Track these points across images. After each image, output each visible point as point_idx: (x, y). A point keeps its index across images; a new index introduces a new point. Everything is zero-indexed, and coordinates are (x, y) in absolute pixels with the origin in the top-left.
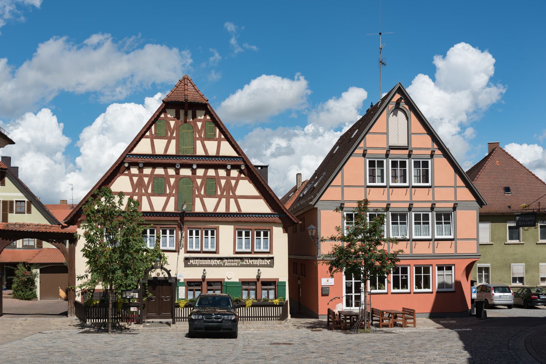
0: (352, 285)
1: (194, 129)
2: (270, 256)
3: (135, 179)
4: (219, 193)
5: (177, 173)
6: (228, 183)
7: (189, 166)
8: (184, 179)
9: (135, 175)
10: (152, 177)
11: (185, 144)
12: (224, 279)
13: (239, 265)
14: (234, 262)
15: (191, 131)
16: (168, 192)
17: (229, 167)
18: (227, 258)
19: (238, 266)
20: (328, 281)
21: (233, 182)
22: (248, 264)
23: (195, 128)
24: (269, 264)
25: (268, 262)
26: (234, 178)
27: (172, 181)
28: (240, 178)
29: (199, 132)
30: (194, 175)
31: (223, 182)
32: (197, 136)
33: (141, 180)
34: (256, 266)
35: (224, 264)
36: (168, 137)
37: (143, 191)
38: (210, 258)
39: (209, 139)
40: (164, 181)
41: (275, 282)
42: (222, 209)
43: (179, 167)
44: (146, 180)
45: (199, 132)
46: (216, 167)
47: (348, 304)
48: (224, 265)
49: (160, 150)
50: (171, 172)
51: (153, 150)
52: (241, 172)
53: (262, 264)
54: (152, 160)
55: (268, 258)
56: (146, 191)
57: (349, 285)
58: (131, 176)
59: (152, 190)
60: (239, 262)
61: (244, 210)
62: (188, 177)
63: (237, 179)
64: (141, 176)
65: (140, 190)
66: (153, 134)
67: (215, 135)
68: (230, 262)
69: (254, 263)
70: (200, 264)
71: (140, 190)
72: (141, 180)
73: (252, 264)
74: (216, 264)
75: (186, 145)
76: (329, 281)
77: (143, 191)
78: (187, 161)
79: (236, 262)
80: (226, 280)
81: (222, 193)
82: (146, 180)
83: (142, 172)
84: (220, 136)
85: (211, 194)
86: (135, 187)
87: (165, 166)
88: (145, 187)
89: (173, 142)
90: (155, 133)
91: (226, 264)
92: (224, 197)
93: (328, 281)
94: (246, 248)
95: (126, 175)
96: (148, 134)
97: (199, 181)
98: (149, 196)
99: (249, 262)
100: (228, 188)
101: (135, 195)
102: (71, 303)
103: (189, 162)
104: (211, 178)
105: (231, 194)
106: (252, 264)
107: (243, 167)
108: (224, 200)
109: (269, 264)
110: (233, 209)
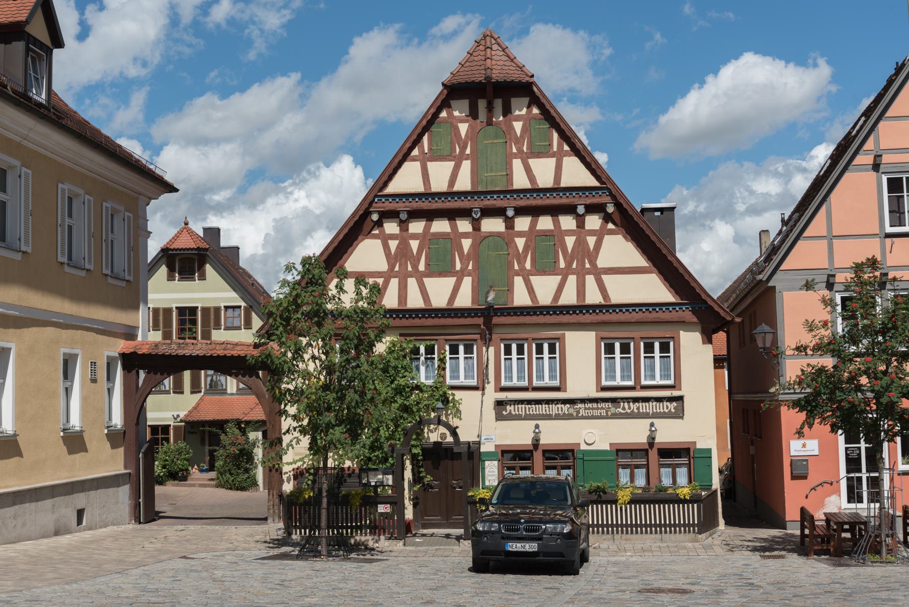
0: (860, 454)
1: (508, 137)
2: (676, 393)
3: (393, 245)
4: (562, 264)
5: (477, 228)
6: (581, 243)
7: (498, 212)
8: (490, 238)
9: (393, 237)
10: (426, 238)
11: (489, 168)
12: (579, 444)
13: (609, 413)
14: (598, 409)
15: (501, 141)
16: (458, 266)
17: (510, 213)
18: (583, 401)
19: (607, 417)
20: (804, 446)
21: (591, 241)
22: (629, 411)
23: (510, 134)
24: (673, 410)
25: (672, 406)
26: (592, 233)
27: (466, 244)
28: (605, 232)
29: (518, 141)
30: (511, 231)
31: (570, 241)
32: (514, 150)
33: (404, 247)
34: (646, 416)
35: (578, 412)
36: (455, 157)
37: (410, 269)
38: (548, 402)
39: (539, 155)
40: (449, 245)
41: (689, 449)
42: (569, 297)
43: (479, 215)
44: (414, 245)
45: (518, 141)
46: (555, 211)
47: (854, 495)
48: (577, 415)
49: (439, 184)
50: (464, 226)
51: (427, 183)
52: (607, 218)
53: (658, 411)
54: (425, 205)
55: (671, 399)
56: (415, 267)
57: (854, 455)
58: (385, 239)
59: (427, 265)
60: (609, 408)
61: (615, 299)
62: (498, 235)
63: (600, 235)
64: (404, 237)
65: (403, 266)
66: (426, 151)
67: (551, 145)
68: (589, 409)
69: (641, 411)
70: (528, 413)
71: (403, 266)
72: (404, 247)
73: (636, 411)
74: (560, 412)
75: (491, 171)
76: (807, 446)
77: (410, 269)
78: (494, 202)
79: (602, 408)
80: (583, 447)
81: (569, 264)
82: (414, 245)
83: (407, 230)
84: (560, 146)
85: (545, 268)
86: (568, 258)
87: (452, 215)
88: (412, 259)
89: (466, 165)
90: (430, 149)
91: (582, 413)
92: (573, 274)
93: (804, 446)
94: (623, 378)
95: (376, 237)
96: (415, 152)
97: (520, 242)
98: (420, 277)
99: (629, 408)
100: (580, 253)
101: (394, 277)
102: (273, 495)
103: (499, 203)
104: (546, 234)
105: (587, 266)
106: (636, 411)
107: (610, 209)
108: (572, 279)
109: (673, 410)
110: (593, 297)
